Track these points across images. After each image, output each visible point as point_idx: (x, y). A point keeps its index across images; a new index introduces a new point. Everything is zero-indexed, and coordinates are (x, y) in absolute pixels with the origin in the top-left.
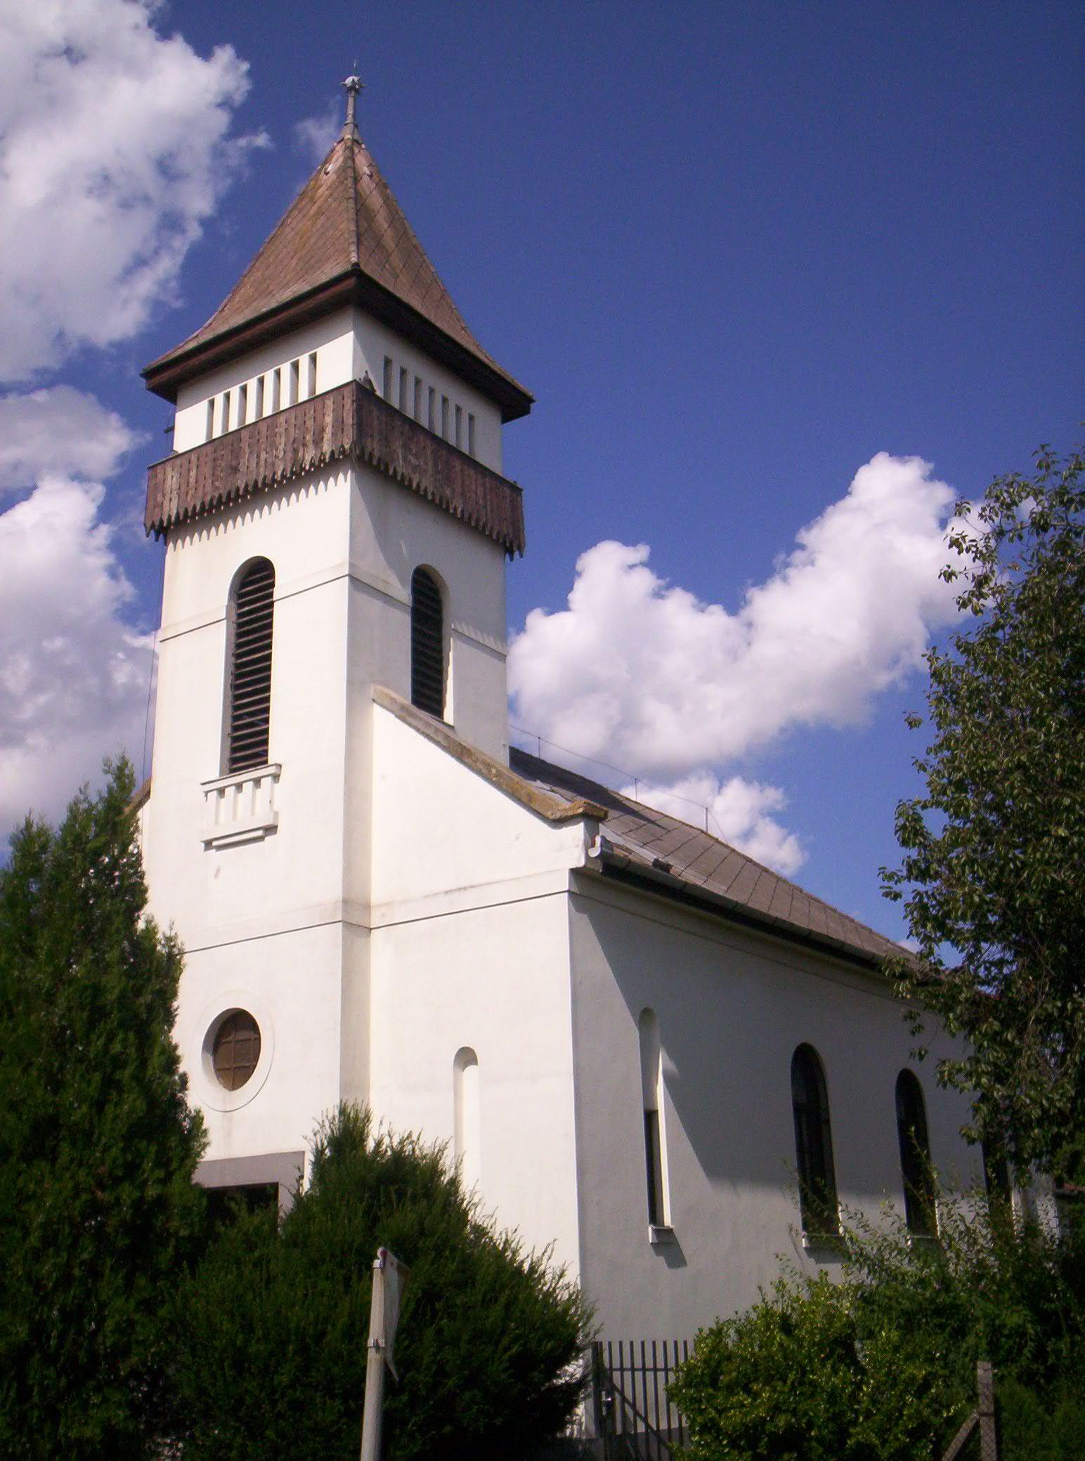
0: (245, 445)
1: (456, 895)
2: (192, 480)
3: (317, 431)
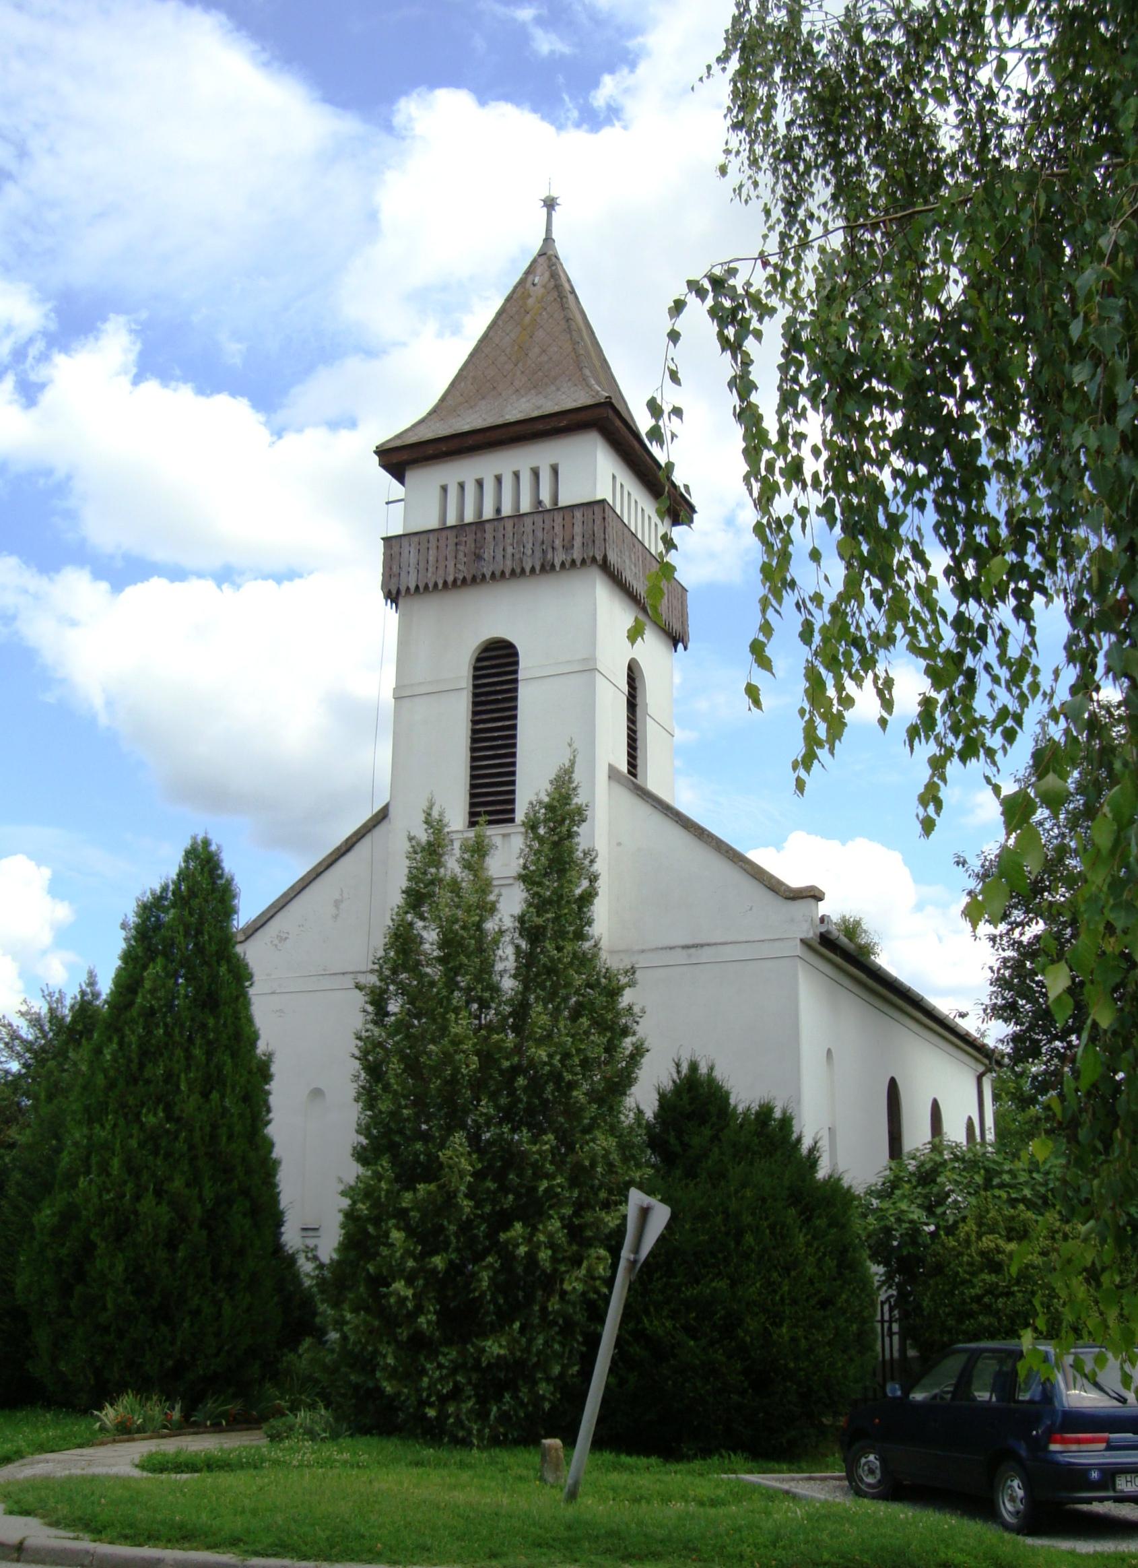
0: (489, 536)
1: (693, 951)
2: (431, 559)
3: (567, 539)
